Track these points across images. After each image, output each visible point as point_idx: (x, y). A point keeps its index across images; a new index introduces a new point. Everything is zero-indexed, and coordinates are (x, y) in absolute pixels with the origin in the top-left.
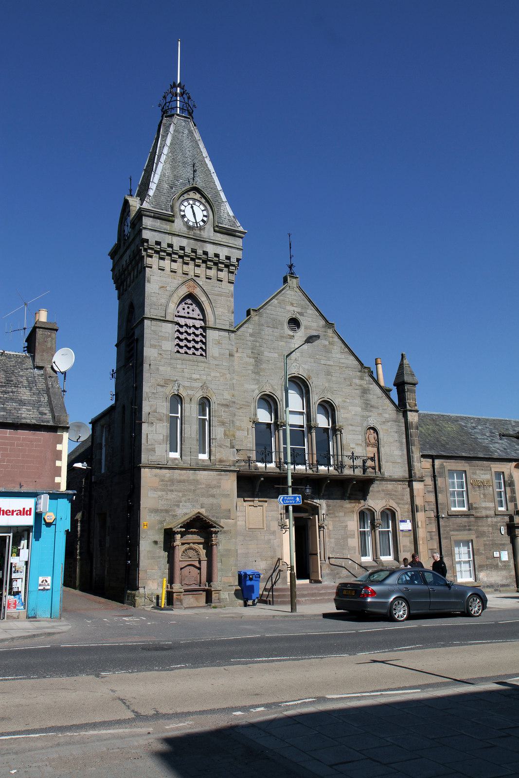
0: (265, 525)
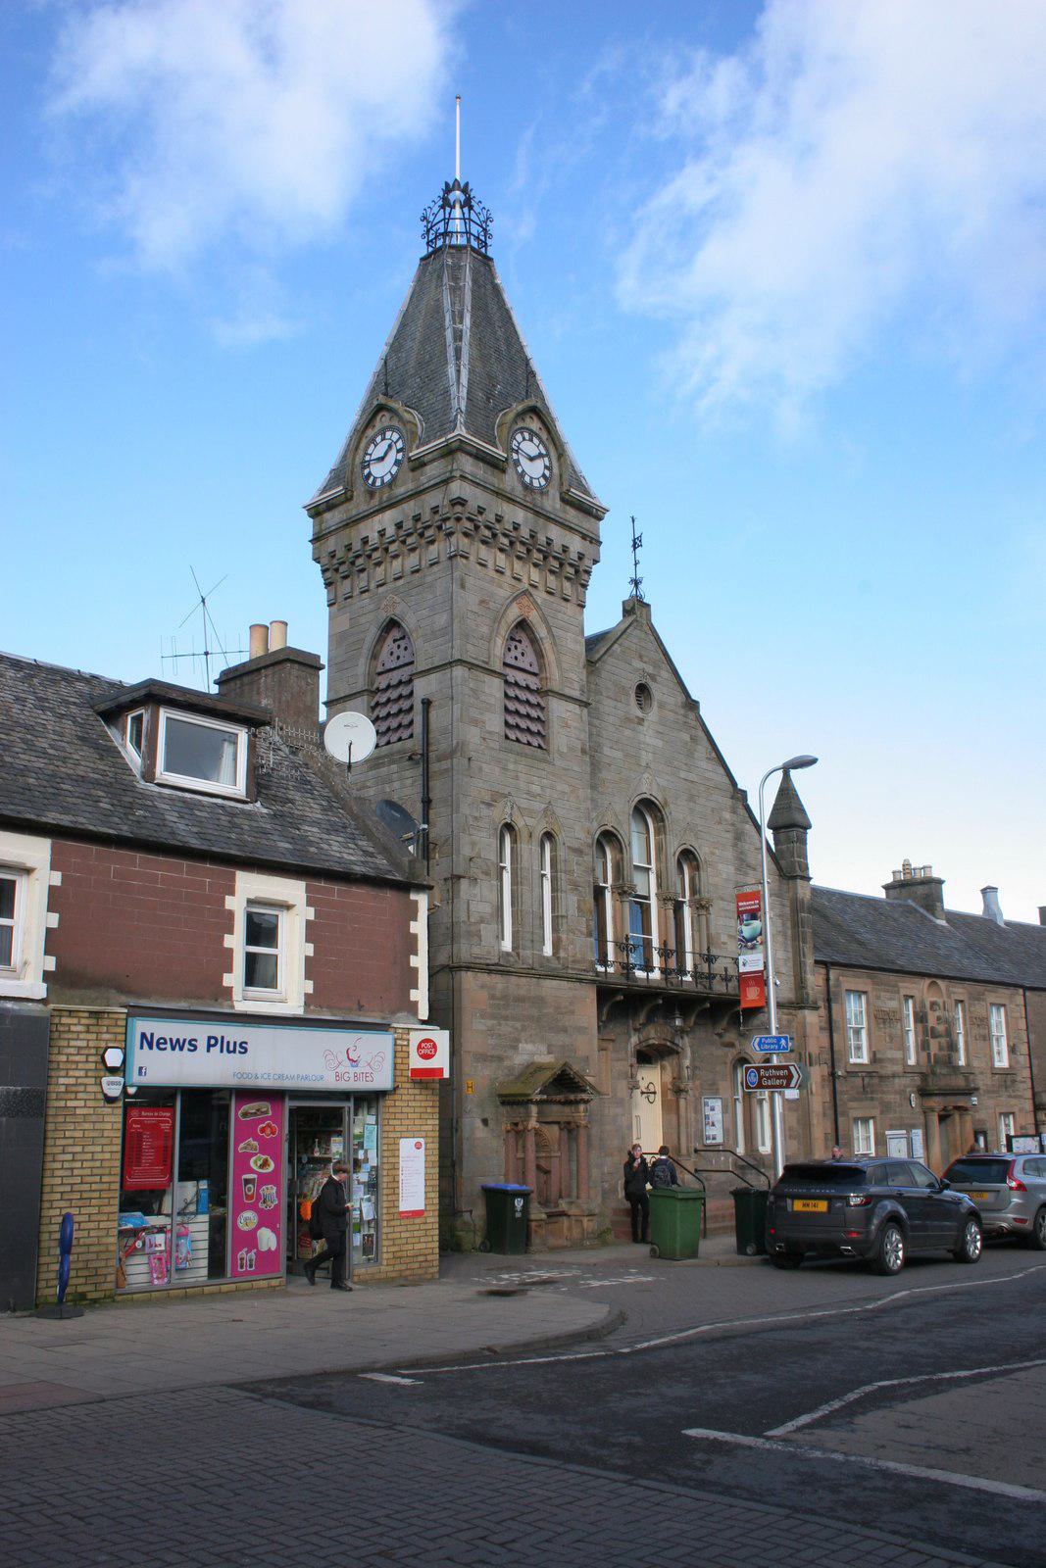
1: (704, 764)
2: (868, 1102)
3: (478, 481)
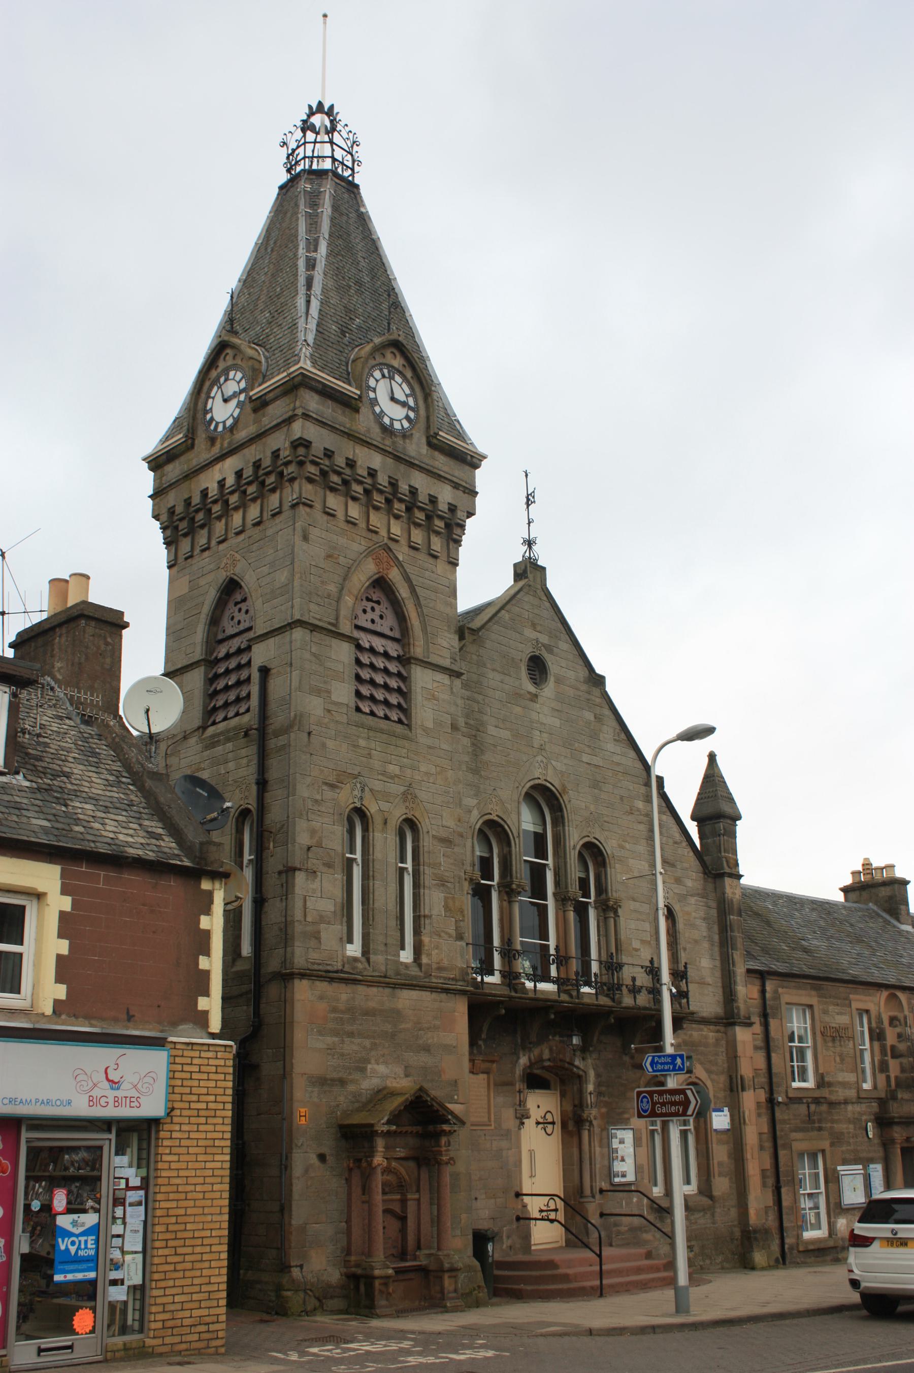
0: (493, 1119)
1: (611, 747)
2: (816, 1133)
3: (324, 420)
